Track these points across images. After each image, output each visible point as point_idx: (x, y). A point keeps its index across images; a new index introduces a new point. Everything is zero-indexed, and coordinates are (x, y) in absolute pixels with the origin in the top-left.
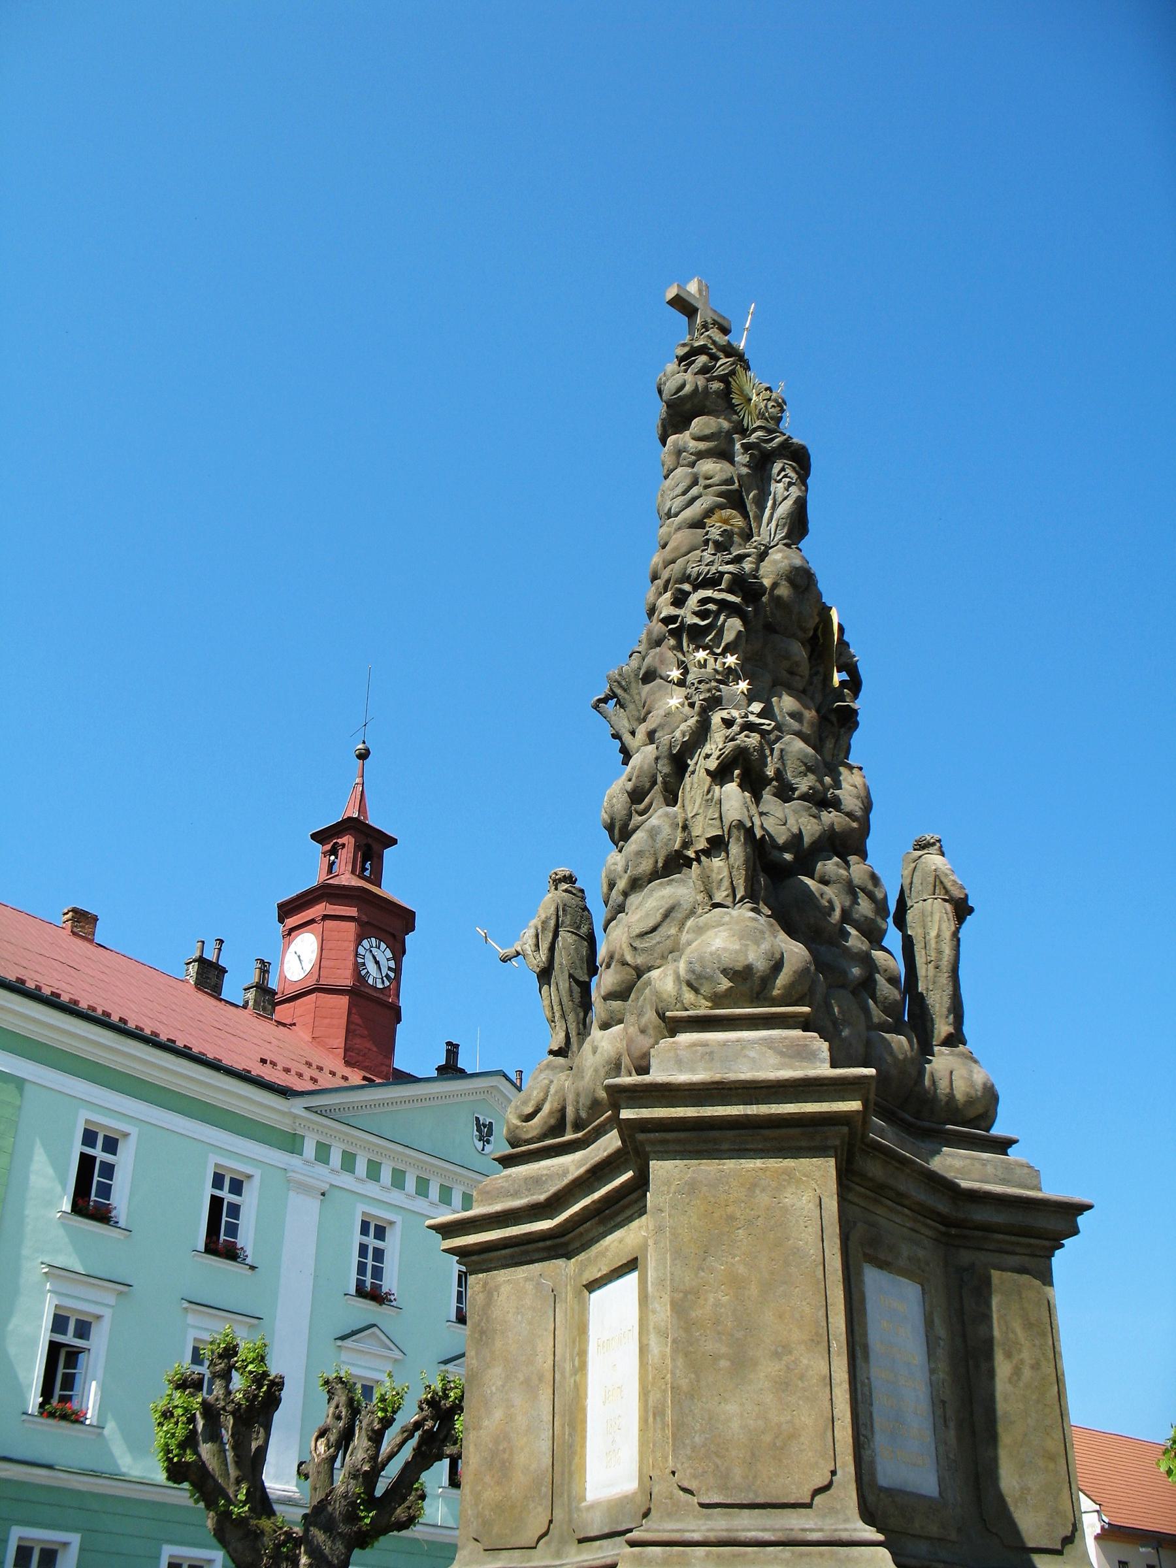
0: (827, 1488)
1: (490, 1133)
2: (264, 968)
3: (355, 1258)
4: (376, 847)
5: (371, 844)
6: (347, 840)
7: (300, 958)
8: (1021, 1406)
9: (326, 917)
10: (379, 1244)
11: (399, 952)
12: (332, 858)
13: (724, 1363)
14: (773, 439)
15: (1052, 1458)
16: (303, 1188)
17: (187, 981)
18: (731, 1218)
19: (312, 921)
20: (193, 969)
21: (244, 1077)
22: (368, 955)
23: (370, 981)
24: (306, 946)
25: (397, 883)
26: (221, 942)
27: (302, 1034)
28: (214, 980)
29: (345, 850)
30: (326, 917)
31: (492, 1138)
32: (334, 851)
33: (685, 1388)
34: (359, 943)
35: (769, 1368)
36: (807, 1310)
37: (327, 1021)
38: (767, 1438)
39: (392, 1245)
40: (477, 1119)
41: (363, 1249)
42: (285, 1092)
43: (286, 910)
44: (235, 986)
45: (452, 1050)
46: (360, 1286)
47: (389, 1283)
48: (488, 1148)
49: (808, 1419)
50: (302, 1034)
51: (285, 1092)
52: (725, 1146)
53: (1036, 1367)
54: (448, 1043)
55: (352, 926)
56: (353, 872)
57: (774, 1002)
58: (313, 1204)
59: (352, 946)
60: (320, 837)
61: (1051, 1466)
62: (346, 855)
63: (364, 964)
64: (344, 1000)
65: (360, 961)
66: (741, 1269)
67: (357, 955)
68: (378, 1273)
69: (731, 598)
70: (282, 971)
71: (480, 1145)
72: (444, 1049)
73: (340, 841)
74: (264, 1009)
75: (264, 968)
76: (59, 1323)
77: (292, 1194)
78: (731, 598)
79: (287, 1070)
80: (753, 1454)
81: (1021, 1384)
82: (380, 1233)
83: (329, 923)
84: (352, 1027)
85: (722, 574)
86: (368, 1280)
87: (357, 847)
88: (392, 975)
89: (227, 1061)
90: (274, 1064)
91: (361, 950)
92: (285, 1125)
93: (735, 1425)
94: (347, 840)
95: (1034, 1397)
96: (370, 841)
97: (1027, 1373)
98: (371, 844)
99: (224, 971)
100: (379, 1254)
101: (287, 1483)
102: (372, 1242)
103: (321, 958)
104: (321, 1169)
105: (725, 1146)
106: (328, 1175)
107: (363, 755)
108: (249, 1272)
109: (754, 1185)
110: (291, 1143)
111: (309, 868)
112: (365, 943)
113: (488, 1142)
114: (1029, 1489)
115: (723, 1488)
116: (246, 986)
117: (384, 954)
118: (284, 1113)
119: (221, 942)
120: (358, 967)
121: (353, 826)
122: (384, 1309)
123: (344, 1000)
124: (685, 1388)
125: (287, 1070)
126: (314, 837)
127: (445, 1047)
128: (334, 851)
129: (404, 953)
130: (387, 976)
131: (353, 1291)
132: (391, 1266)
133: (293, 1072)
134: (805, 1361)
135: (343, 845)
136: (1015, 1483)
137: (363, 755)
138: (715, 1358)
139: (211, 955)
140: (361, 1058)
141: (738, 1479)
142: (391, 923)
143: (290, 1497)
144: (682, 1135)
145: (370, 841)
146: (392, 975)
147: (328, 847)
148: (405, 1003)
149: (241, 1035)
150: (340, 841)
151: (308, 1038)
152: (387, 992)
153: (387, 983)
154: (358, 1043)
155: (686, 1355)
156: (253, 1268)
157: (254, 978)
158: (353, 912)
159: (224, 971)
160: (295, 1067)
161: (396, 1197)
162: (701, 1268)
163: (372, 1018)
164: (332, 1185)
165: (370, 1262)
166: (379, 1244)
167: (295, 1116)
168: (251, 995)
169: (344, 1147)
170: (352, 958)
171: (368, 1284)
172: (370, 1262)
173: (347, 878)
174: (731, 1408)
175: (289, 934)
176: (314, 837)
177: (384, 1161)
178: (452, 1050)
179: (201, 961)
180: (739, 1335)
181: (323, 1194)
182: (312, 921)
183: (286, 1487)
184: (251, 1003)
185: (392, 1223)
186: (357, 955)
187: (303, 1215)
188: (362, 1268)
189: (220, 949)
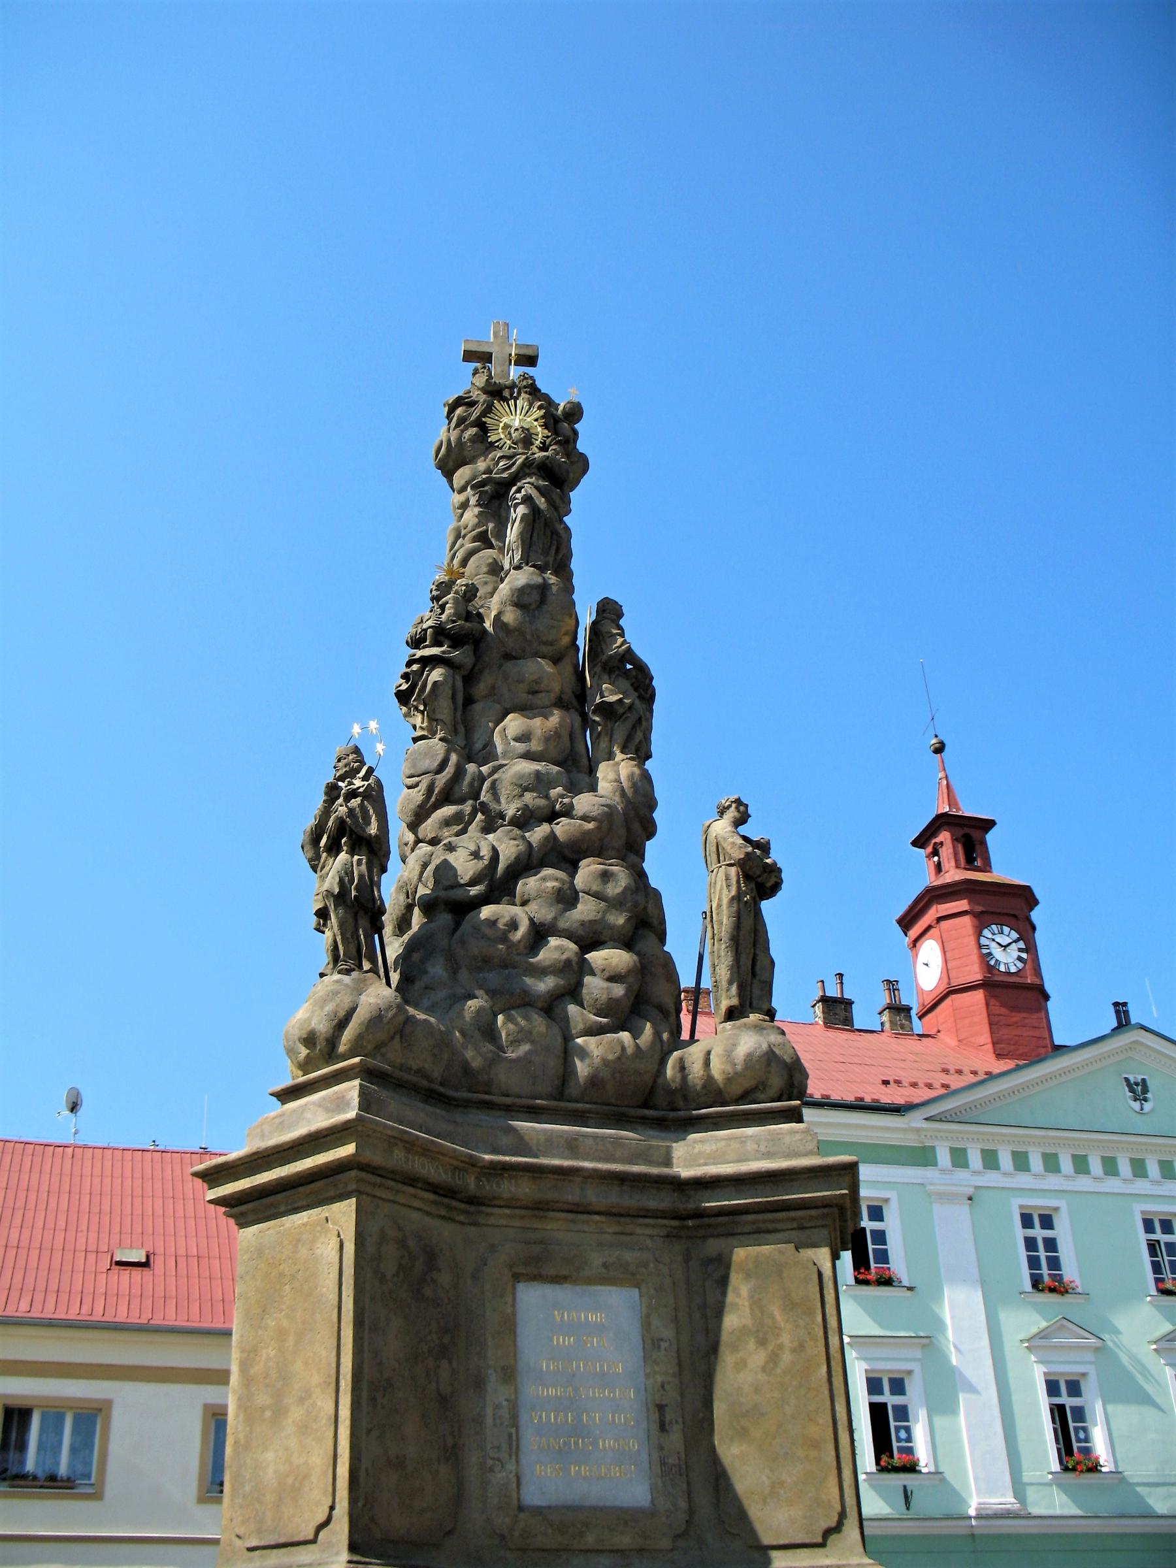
0: (327, 1522)
1: (1145, 1090)
2: (892, 986)
3: (1022, 1254)
4: (975, 834)
5: (971, 835)
6: (944, 836)
7: (928, 967)
8: (776, 1394)
9: (940, 919)
10: (1048, 1233)
11: (1026, 932)
12: (936, 859)
13: (268, 1414)
14: (514, 463)
15: (815, 1445)
16: (947, 1198)
17: (817, 1023)
18: (282, 1275)
19: (929, 927)
20: (819, 1009)
21: (858, 1106)
22: (993, 945)
23: (1002, 968)
24: (930, 950)
25: (1005, 866)
26: (841, 975)
27: (948, 1039)
28: (842, 1014)
29: (944, 848)
30: (940, 919)
31: (1149, 1095)
32: (935, 853)
33: (242, 1442)
34: (979, 934)
35: (296, 1414)
36: (324, 1353)
37: (967, 1021)
38: (290, 1481)
39: (1062, 1232)
40: (1127, 1080)
41: (1030, 1244)
42: (896, 1110)
43: (906, 922)
44: (868, 1010)
45: (1121, 1009)
46: (1036, 1283)
47: (1070, 1271)
48: (1147, 1106)
49: (318, 1459)
50: (948, 1039)
51: (896, 1110)
52: (282, 1209)
53: (800, 1348)
54: (1116, 1004)
55: (967, 919)
56: (957, 867)
57: (345, 1057)
58: (962, 1211)
59: (971, 940)
60: (920, 842)
61: (814, 1454)
62: (946, 852)
63: (990, 954)
64: (979, 996)
65: (985, 951)
66: (285, 1323)
67: (980, 946)
68: (1054, 1263)
69: (435, 651)
70: (917, 984)
71: (1136, 1105)
72: (1111, 1010)
73: (937, 840)
74: (902, 1026)
75: (892, 986)
76: (1052, 1388)
77: (936, 1208)
78: (435, 651)
79: (914, 1085)
80: (280, 1498)
81: (779, 1371)
82: (1047, 1222)
83: (944, 924)
84: (996, 1019)
85: (426, 630)
86: (1045, 1271)
87: (955, 840)
88: (1024, 955)
89: (835, 1097)
90: (898, 1082)
91: (983, 941)
92: (911, 1141)
93: (270, 1471)
94: (944, 836)
95: (794, 1383)
96: (967, 830)
97: (787, 1357)
98: (971, 835)
99: (849, 1003)
100: (1051, 1244)
101: (1003, 1495)
102: (1038, 1233)
103: (946, 961)
104: (961, 1174)
105: (282, 1209)
106: (972, 1177)
107: (939, 749)
108: (909, 1293)
109: (298, 1241)
110: (923, 1157)
111: (919, 873)
112: (986, 932)
113: (1146, 1100)
114: (782, 1483)
115: (259, 1531)
116: (880, 1009)
117: (1008, 935)
118: (904, 1130)
119: (841, 975)
120: (985, 958)
121: (941, 822)
122: (1068, 1298)
123: (979, 996)
124: (242, 1442)
125: (914, 1085)
126: (915, 843)
127: (1112, 1009)
128: (935, 853)
129: (1034, 928)
130: (1020, 959)
131: (1027, 1285)
132: (1067, 1254)
133: (921, 1085)
134: (319, 1404)
135: (942, 843)
136: (764, 1478)
137: (939, 749)
138: (263, 1409)
139: (833, 992)
140: (1012, 1048)
141: (269, 1523)
142: (1011, 906)
143: (1008, 1510)
144: (250, 1206)
145: (967, 830)
146: (1024, 955)
147: (930, 849)
148: (1048, 987)
149: (869, 1061)
150: (937, 840)
151: (953, 1042)
152: (1021, 974)
153: (1020, 965)
154: (1005, 1032)
155: (245, 1410)
156: (910, 1289)
157: (884, 999)
158: (962, 905)
159: (849, 1003)
160: (921, 1079)
161: (1053, 1182)
162: (260, 1327)
163: (1016, 1004)
164: (977, 1188)
165: (1042, 1254)
166: (1048, 1233)
167: (918, 1130)
168: (885, 1017)
169: (980, 1146)
170: (975, 951)
171: (1046, 1279)
172: (1042, 1254)
173: (953, 874)
174: (270, 1455)
175: (914, 946)
176: (915, 843)
177: (1030, 1149)
178: (1121, 1009)
179: (825, 1000)
180: (279, 1385)
181: (970, 1199)
182: (929, 927)
183: (1003, 1500)
184: (887, 1025)
185: (1056, 1209)
186: (980, 946)
187: (954, 1227)
188: (1033, 1263)
189: (842, 983)
